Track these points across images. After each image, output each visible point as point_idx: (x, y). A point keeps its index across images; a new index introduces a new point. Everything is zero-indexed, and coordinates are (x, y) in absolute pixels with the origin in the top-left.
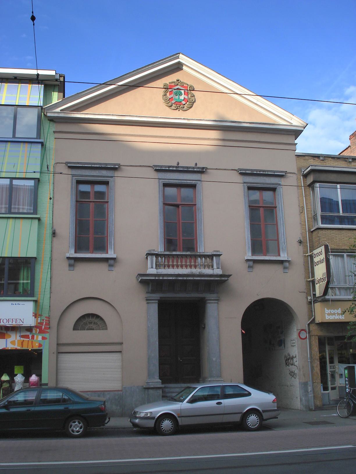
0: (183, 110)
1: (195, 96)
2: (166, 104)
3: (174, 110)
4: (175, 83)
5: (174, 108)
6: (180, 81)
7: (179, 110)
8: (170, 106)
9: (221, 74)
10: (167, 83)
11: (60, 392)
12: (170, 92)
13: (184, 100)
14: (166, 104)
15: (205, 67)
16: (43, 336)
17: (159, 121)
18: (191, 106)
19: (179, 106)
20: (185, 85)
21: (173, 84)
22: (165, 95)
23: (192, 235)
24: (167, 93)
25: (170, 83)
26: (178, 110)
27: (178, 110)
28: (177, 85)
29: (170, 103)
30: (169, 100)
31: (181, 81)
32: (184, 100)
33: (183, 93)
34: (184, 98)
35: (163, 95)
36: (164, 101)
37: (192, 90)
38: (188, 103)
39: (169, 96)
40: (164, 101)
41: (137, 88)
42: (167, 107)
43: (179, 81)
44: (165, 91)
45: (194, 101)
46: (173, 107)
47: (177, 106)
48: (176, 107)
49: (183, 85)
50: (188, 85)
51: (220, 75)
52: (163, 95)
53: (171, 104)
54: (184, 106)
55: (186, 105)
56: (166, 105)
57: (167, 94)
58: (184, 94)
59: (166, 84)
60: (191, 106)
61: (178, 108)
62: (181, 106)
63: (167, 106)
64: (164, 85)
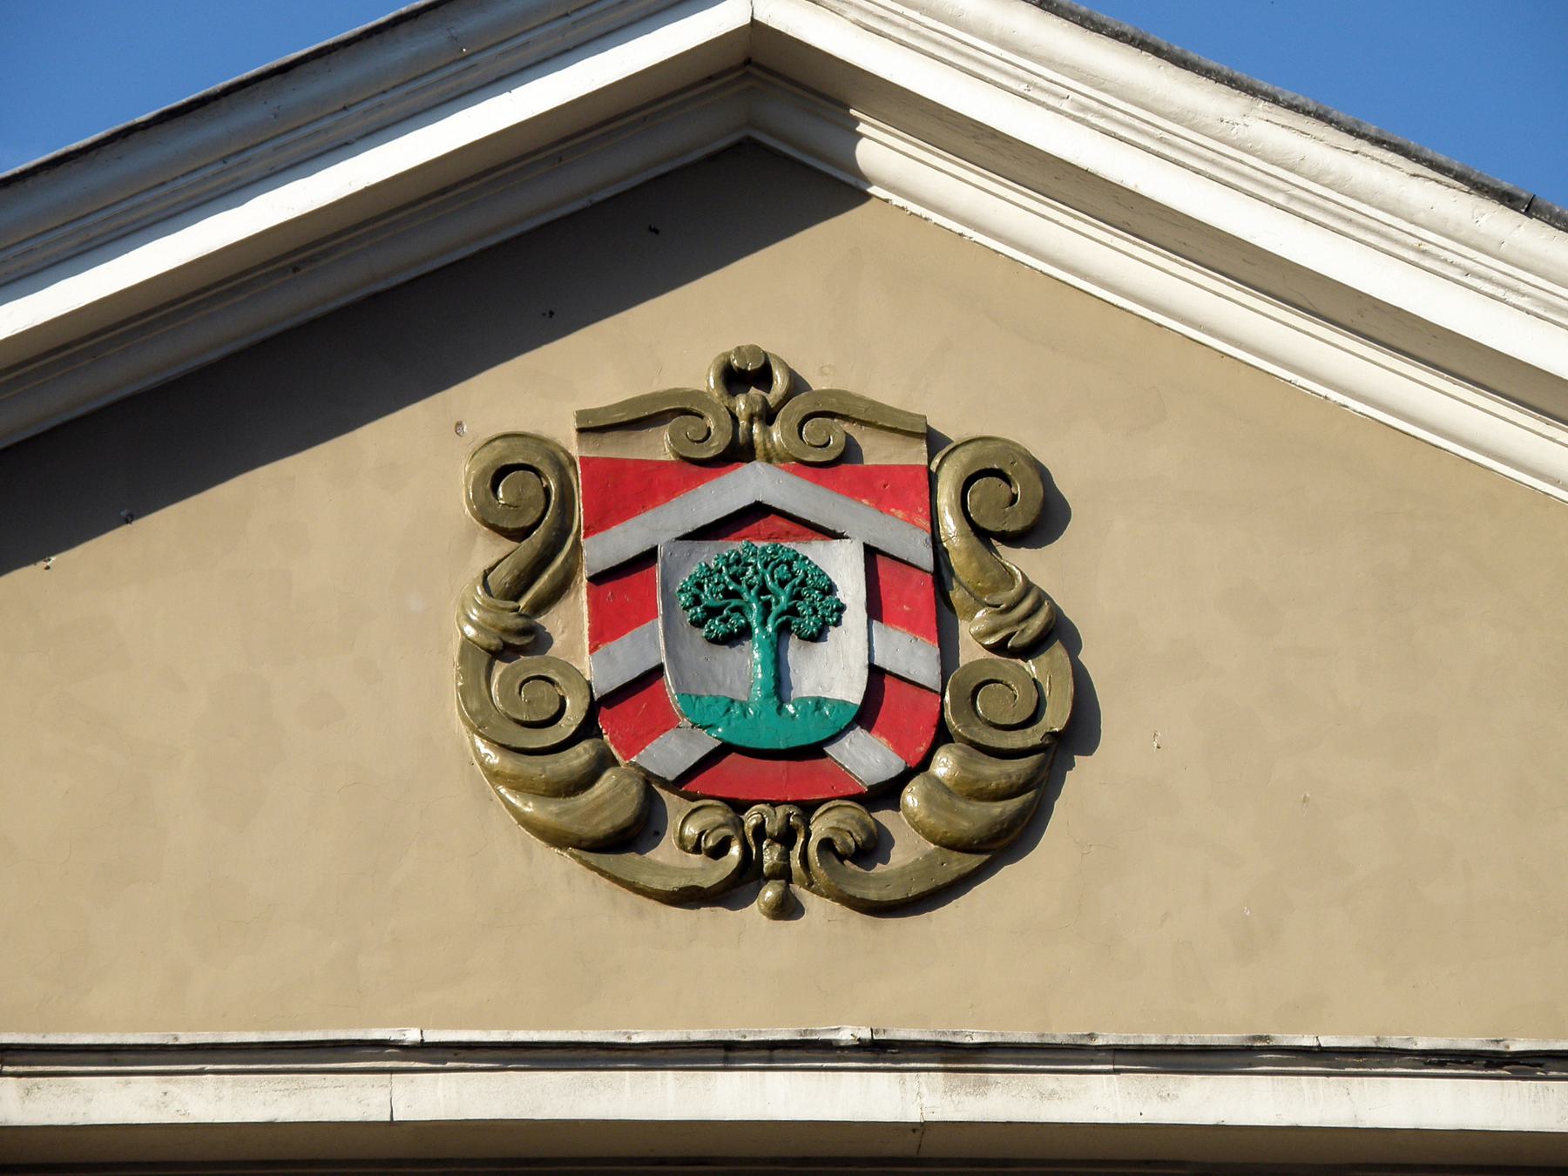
0: (873, 894)
1: (1073, 643)
2: (529, 808)
3: (689, 898)
4: (690, 427)
5: (697, 860)
6: (780, 382)
7: (786, 909)
8: (603, 825)
9: (1544, 199)
10: (546, 431)
11: (735, 464)
12: (597, 579)
13: (866, 715)
14: (529, 808)
15: (1242, 101)
16: (600, 740)
17: (405, 1112)
18: (998, 809)
19: (772, 827)
20: (879, 451)
21: (659, 446)
22: (504, 652)
23: (806, 884)
24: (544, 603)
25: (590, 429)
26: (769, 893)
27: (769, 893)
28: (738, 453)
29: (608, 778)
30: (588, 729)
31: (797, 385)
32: (866, 715)
33: (851, 587)
34: (876, 674)
35: (467, 644)
36: (494, 758)
37: (1015, 539)
38: (944, 765)
39: (587, 665)
40: (505, 748)
41: (711, 478)
42: (561, 862)
43: (763, 377)
44: (501, 577)
45: (1056, 718)
46: (666, 852)
47: (751, 819)
48: (735, 850)
49: (850, 452)
50: (935, 441)
51: (1535, 224)
52: (467, 644)
53: (635, 790)
54: (884, 817)
55: (911, 797)
56: (527, 823)
57: (552, 621)
58: (875, 609)
59: (539, 441)
60: (998, 809)
61: (770, 857)
62: (820, 827)
63: (557, 839)
64: (490, 458)
